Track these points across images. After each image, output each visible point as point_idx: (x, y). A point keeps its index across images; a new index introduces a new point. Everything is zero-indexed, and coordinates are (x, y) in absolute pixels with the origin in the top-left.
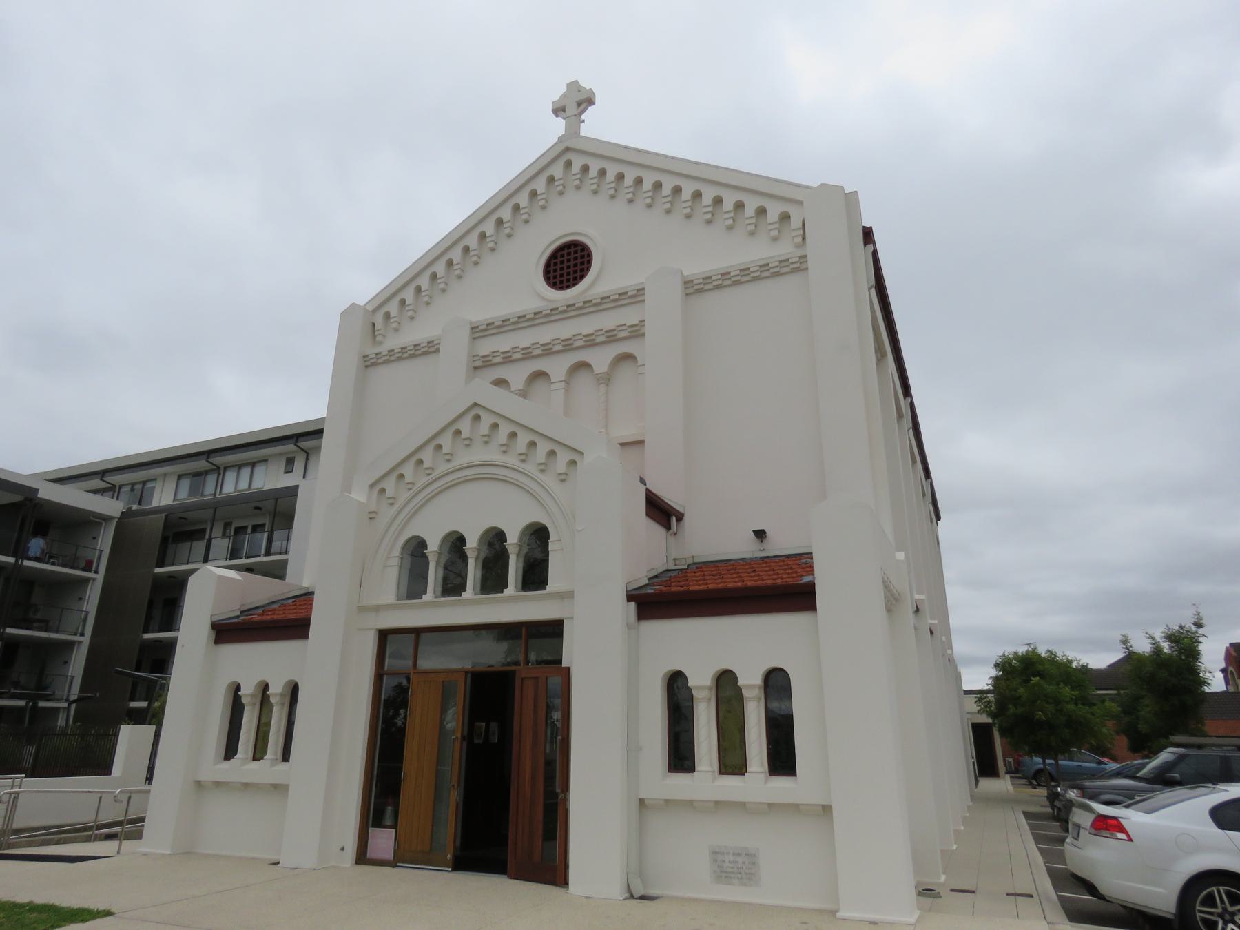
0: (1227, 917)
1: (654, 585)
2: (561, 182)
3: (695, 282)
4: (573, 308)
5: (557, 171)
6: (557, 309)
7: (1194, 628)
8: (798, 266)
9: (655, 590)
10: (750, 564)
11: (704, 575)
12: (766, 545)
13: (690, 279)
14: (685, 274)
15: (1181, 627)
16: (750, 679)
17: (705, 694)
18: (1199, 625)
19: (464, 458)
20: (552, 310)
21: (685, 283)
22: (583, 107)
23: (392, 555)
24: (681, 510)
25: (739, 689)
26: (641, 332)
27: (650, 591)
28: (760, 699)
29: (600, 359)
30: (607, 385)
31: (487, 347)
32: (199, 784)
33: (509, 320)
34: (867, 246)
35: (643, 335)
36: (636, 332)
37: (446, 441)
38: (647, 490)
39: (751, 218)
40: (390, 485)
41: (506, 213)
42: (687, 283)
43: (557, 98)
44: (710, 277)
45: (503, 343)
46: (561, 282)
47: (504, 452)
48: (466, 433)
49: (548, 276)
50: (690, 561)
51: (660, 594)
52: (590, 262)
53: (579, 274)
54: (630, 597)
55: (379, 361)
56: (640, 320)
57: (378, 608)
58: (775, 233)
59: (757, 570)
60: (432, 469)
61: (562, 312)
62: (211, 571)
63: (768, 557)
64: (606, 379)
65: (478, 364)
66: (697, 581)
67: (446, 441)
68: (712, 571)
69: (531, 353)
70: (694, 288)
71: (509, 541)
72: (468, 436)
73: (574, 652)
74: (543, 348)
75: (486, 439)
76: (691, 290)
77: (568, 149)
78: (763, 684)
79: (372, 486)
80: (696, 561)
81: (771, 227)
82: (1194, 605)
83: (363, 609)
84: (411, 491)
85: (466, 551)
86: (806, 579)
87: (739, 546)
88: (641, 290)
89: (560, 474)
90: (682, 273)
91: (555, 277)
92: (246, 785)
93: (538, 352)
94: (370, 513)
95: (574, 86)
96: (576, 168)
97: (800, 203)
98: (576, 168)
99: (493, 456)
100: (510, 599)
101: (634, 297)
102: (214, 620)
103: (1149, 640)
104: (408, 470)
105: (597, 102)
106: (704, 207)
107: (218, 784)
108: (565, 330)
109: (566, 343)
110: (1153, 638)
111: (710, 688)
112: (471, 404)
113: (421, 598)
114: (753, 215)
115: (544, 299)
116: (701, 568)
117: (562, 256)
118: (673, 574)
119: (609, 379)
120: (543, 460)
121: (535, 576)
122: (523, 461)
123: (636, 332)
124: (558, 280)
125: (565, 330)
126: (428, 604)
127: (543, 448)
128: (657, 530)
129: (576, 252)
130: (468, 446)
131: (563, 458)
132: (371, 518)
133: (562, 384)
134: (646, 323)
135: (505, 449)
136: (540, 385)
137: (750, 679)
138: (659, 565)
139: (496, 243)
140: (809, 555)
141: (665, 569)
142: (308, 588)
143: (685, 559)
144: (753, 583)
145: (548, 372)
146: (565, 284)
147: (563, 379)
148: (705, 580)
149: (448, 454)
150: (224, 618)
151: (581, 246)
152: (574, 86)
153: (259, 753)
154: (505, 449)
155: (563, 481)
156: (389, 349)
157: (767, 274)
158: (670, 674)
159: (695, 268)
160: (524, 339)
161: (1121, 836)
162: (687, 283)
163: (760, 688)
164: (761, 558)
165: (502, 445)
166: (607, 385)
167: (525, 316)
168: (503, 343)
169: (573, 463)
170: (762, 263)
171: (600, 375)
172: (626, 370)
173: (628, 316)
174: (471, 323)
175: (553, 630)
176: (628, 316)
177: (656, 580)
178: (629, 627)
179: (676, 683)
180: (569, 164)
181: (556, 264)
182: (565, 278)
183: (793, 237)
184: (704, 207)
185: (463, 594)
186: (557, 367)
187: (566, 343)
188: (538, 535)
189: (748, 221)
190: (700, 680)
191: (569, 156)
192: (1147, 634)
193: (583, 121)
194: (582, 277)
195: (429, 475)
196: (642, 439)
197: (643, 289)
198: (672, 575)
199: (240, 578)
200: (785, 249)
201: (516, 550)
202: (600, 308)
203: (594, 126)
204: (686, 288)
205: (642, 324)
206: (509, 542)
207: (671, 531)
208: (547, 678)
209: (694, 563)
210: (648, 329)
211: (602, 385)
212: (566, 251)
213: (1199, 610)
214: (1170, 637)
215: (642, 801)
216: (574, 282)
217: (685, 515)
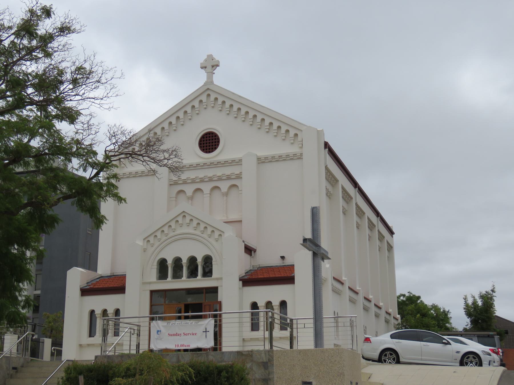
0: (389, 359)
1: (247, 276)
2: (205, 104)
5: (204, 98)
8: (299, 157)
9: (248, 277)
10: (279, 268)
11: (263, 272)
12: (284, 261)
13: (260, 157)
14: (258, 155)
15: (486, 292)
18: (493, 291)
19: (179, 231)
21: (258, 159)
23: (154, 264)
24: (255, 248)
25: (273, 306)
26: (241, 177)
27: (246, 278)
28: (278, 309)
29: (224, 186)
30: (227, 196)
32: (81, 345)
34: (326, 149)
35: (242, 178)
36: (239, 177)
37: (173, 224)
38: (245, 244)
39: (283, 134)
40: (151, 239)
41: (181, 114)
43: (202, 62)
44: (267, 158)
46: (206, 149)
47: (195, 229)
48: (180, 222)
49: (201, 146)
50: (258, 266)
51: (249, 279)
52: (219, 142)
54: (240, 280)
55: (125, 177)
56: (240, 172)
57: (150, 283)
58: (292, 141)
59: (280, 271)
60: (167, 234)
61: (208, 165)
62: (78, 269)
63: (285, 265)
64: (226, 194)
65: (172, 183)
66: (261, 274)
67: (173, 224)
68: (266, 271)
70: (261, 161)
72: (181, 223)
73: (222, 296)
75: (188, 224)
76: (260, 162)
77: (208, 89)
78: (279, 305)
79: (144, 239)
80: (260, 266)
81: (291, 139)
82: (493, 281)
83: (144, 283)
84: (160, 242)
85: (182, 264)
86: (293, 275)
87: (275, 261)
88: (240, 160)
89: (216, 239)
90: (257, 155)
91: (204, 147)
94: (144, 249)
95: (210, 57)
96: (212, 98)
98: (212, 98)
99: (190, 230)
100: (199, 280)
101: (238, 162)
102: (81, 287)
103: (473, 299)
104: (159, 234)
105: (220, 65)
106: (266, 126)
107: (89, 345)
108: (210, 173)
110: (474, 297)
112: (182, 211)
113: (181, 279)
114: (285, 133)
116: (262, 269)
117: (207, 137)
118: (252, 271)
119: (227, 194)
120: (210, 234)
121: (208, 273)
122: (202, 233)
123: (239, 177)
124: (205, 148)
125: (210, 173)
126: (184, 281)
127: (209, 229)
128: (248, 256)
129: (212, 137)
130: (181, 226)
131: (217, 233)
132: (144, 251)
133: (174, 199)
134: (243, 173)
135: (195, 229)
136: (198, 195)
137: (276, 303)
138: (248, 268)
139: (176, 127)
140: (294, 265)
141: (250, 269)
142: (101, 275)
143: (257, 266)
144: (278, 275)
146: (208, 150)
147: (209, 193)
148: (263, 274)
149: (174, 229)
150: (83, 286)
151: (215, 134)
152: (210, 57)
154: (195, 229)
155: (217, 241)
156: (130, 172)
158: (252, 303)
159: (262, 153)
161: (369, 342)
162: (259, 159)
163: (279, 306)
164: (283, 266)
165: (195, 227)
166: (227, 196)
167: (192, 165)
169: (220, 235)
171: (224, 193)
172: (234, 191)
175: (214, 290)
177: (247, 274)
178: (240, 289)
179: (254, 306)
180: (209, 95)
181: (204, 141)
182: (208, 147)
183: (299, 144)
184: (266, 126)
185: (182, 278)
186: (206, 188)
188: (208, 260)
189: (282, 135)
191: (208, 92)
192: (472, 295)
195: (167, 236)
196: (241, 220)
197: (242, 160)
198: (253, 272)
199: (85, 271)
201: (201, 264)
204: (258, 161)
205: (241, 173)
206: (198, 261)
207: (252, 256)
208: (213, 305)
209: (260, 267)
210: (243, 176)
211: (224, 197)
212: (208, 136)
213: (494, 284)
214: (482, 297)
215: (244, 339)
216: (212, 150)
217: (257, 250)
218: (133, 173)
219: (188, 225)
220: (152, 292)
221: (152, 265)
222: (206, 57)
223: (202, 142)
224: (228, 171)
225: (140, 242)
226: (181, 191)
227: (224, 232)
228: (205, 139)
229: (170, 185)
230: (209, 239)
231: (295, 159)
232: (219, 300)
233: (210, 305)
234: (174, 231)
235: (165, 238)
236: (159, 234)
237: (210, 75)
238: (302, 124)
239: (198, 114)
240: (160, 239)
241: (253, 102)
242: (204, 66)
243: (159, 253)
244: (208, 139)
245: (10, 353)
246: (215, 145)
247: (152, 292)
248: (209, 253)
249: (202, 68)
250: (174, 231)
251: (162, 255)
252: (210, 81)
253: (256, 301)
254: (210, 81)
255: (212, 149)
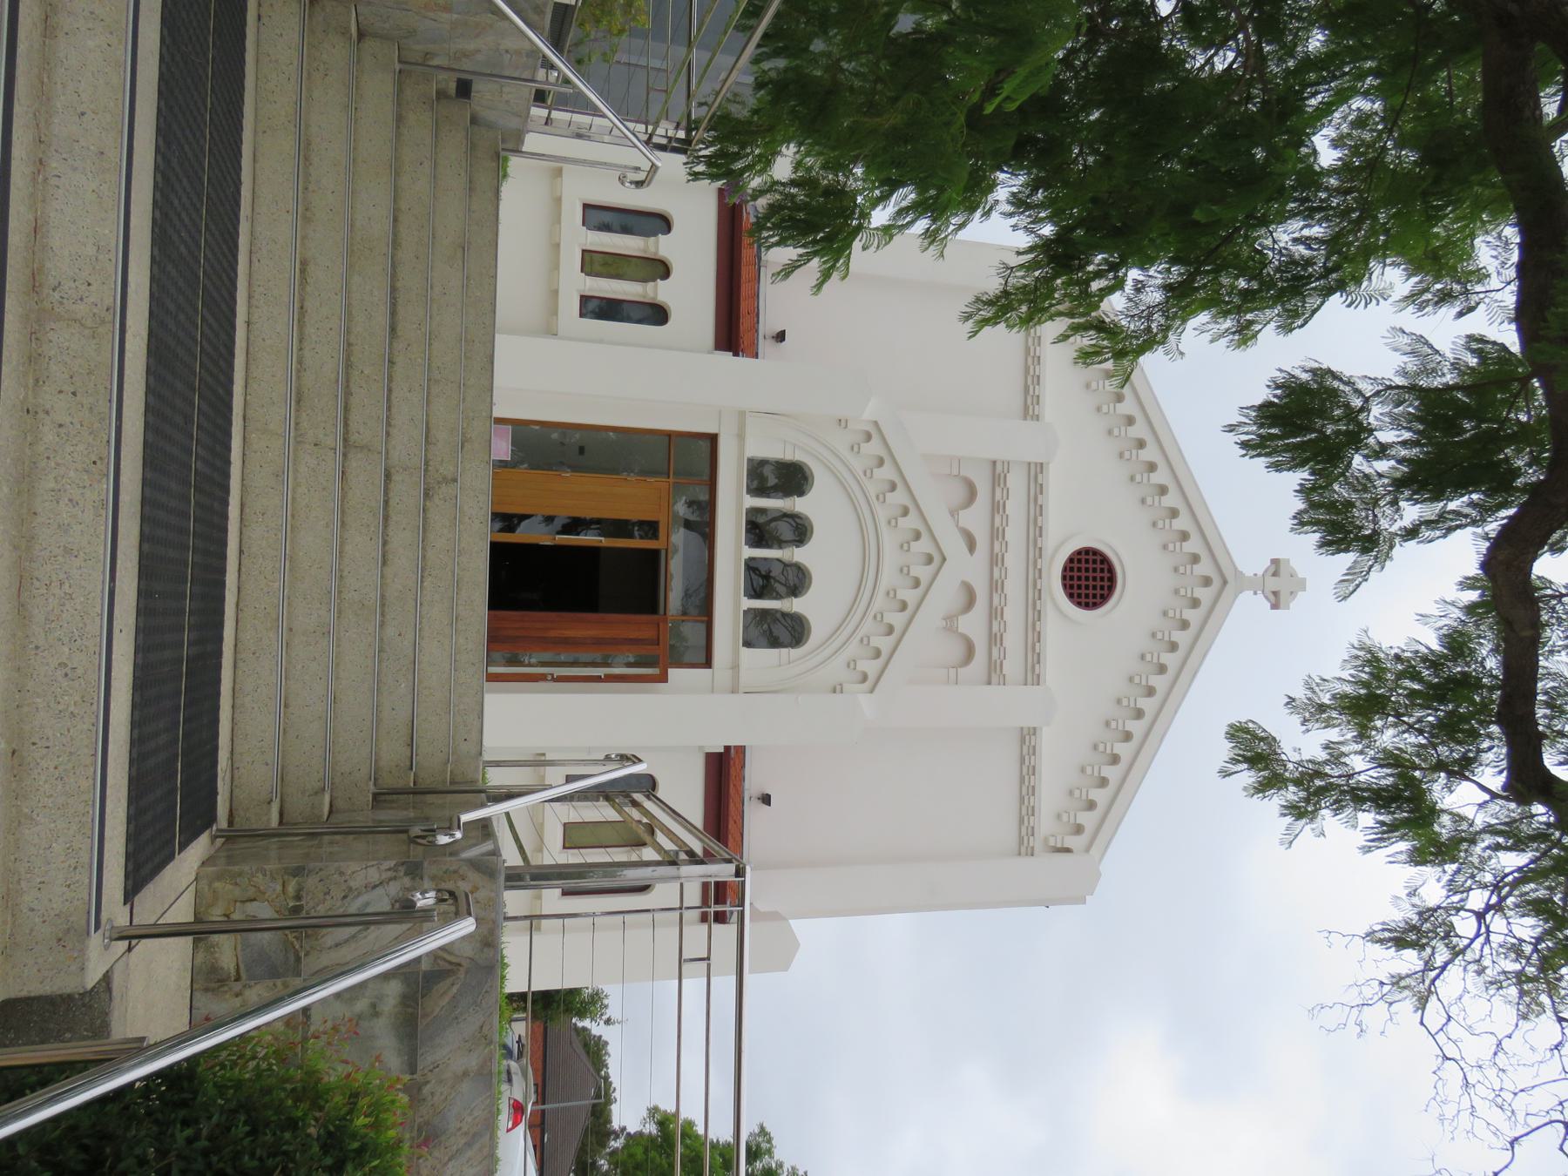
3: (1033, 737)
4: (1037, 576)
5: (1204, 568)
6: (1040, 577)
7: (604, 1017)
16: (662, 291)
17: (652, 249)
19: (889, 541)
20: (1040, 570)
22: (1272, 597)
25: (654, 280)
28: (644, 297)
29: (973, 624)
31: (1016, 483)
33: (1042, 473)
40: (874, 448)
42: (1034, 731)
45: (1016, 507)
47: (888, 593)
53: (1075, 591)
57: (741, 437)
65: (999, 468)
67: (911, 522)
69: (997, 591)
70: (1027, 739)
71: (796, 550)
74: (1001, 502)
75: (905, 570)
77: (1225, 582)
78: (656, 302)
79: (876, 423)
84: (861, 474)
88: (1037, 681)
91: (1079, 561)
92: (557, 247)
93: (997, 548)
97: (1088, 849)
99: (889, 577)
100: (739, 551)
101: (1033, 675)
107: (558, 201)
109: (999, 584)
111: (656, 253)
112: (946, 554)
115: (1056, 550)
117: (1102, 570)
123: (994, 673)
124: (1076, 565)
129: (1102, 588)
131: (871, 667)
133: (955, 472)
135: (891, 593)
137: (662, 291)
145: (969, 509)
153: (594, 263)
154: (891, 593)
157: (1024, 812)
160: (1015, 534)
162: (1034, 731)
163: (654, 298)
168: (1016, 507)
169: (865, 678)
170: (1036, 809)
173: (1013, 665)
174: (1048, 464)
176: (1013, 665)
178: (701, 748)
181: (1095, 562)
187: (999, 584)
190: (663, 246)
193: (1255, 593)
194: (1071, 596)
200: (1046, 824)
202: (1031, 548)
203: (1248, 607)
212: (1106, 575)
218: (1038, 348)
219: (903, 570)
220: (713, 439)
221: (795, 446)
222: (1300, 576)
223: (1091, 557)
224: (1014, 640)
225: (870, 411)
226: (972, 494)
227: (872, 691)
228: (1098, 566)
229: (994, 463)
230: (855, 640)
231: (1020, 829)
232: (673, 673)
233: (658, 644)
234: (889, 522)
235: (872, 492)
236: (886, 472)
237: (1256, 585)
238: (1107, 847)
239: (1143, 501)
240: (871, 477)
241: (1176, 712)
242: (1282, 567)
243: (833, 472)
244: (1098, 575)
245: (504, 89)
246: (1072, 569)
247: (713, 439)
248: (817, 632)
249: (1275, 562)
250: (889, 522)
251: (820, 479)
252: (1245, 583)
253: (669, 323)
254: (1245, 583)
255: (1071, 587)
